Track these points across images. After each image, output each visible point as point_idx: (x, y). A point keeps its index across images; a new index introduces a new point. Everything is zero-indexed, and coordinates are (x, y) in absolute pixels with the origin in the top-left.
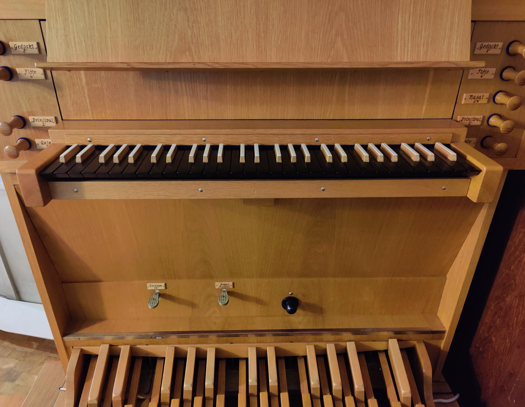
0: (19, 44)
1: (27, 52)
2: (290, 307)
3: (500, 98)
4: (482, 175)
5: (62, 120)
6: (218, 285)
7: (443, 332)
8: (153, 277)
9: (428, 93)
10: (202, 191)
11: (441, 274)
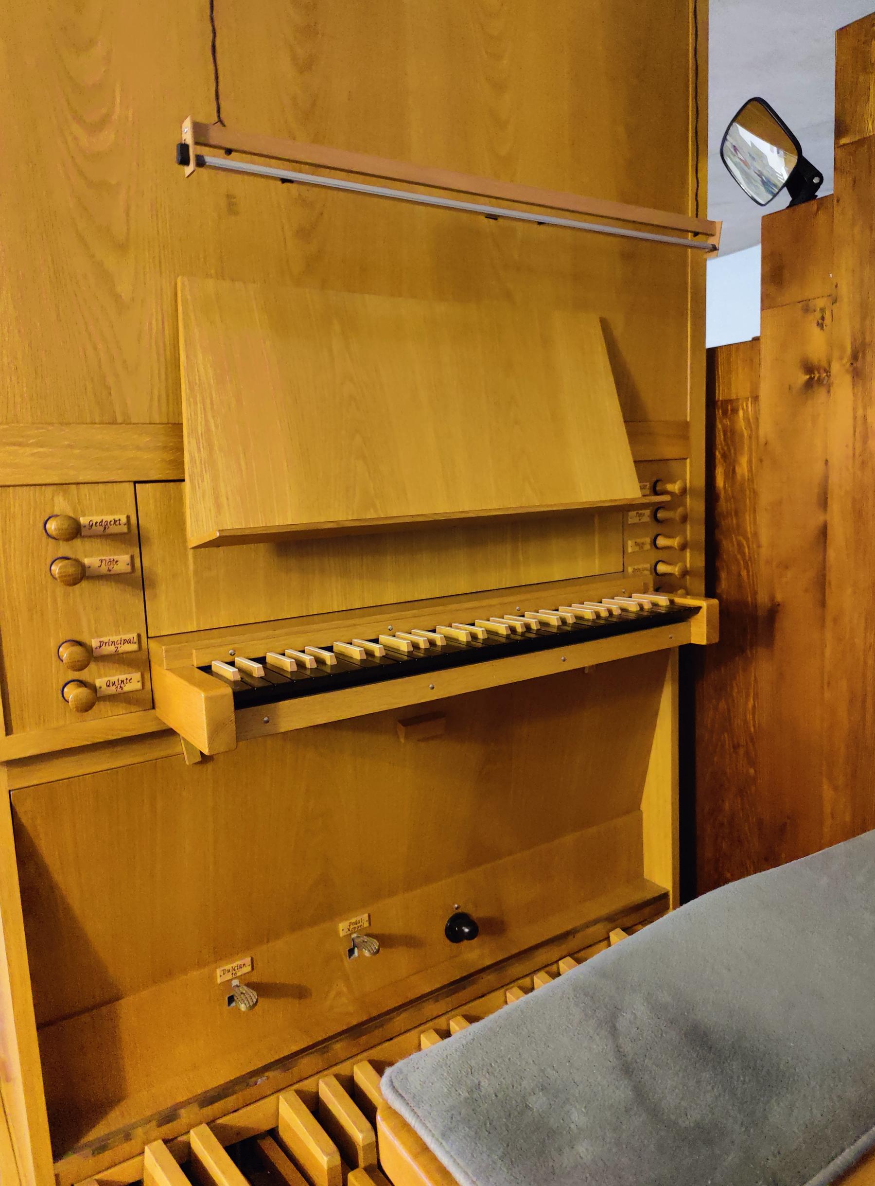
0: (97, 519)
1: (108, 531)
2: (467, 927)
3: (662, 542)
4: (703, 613)
5: (148, 638)
6: (343, 927)
7: (665, 896)
8: (221, 954)
9: (597, 545)
10: (433, 688)
11: (633, 806)
